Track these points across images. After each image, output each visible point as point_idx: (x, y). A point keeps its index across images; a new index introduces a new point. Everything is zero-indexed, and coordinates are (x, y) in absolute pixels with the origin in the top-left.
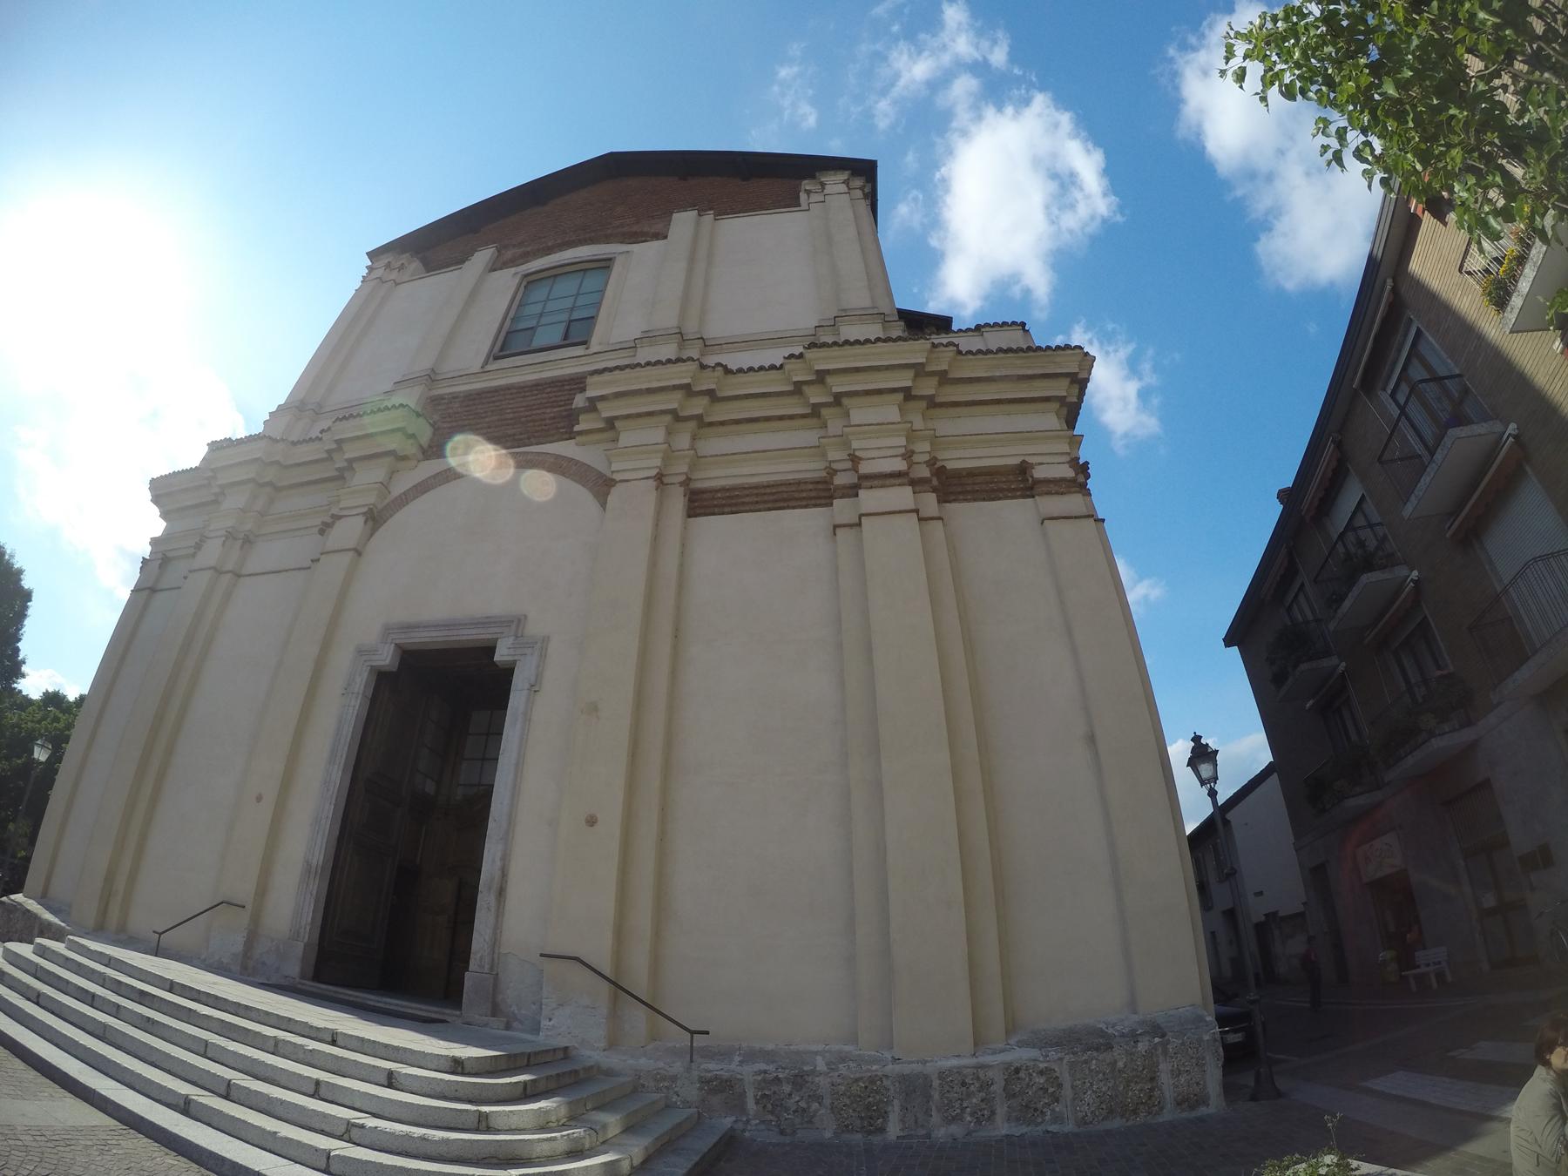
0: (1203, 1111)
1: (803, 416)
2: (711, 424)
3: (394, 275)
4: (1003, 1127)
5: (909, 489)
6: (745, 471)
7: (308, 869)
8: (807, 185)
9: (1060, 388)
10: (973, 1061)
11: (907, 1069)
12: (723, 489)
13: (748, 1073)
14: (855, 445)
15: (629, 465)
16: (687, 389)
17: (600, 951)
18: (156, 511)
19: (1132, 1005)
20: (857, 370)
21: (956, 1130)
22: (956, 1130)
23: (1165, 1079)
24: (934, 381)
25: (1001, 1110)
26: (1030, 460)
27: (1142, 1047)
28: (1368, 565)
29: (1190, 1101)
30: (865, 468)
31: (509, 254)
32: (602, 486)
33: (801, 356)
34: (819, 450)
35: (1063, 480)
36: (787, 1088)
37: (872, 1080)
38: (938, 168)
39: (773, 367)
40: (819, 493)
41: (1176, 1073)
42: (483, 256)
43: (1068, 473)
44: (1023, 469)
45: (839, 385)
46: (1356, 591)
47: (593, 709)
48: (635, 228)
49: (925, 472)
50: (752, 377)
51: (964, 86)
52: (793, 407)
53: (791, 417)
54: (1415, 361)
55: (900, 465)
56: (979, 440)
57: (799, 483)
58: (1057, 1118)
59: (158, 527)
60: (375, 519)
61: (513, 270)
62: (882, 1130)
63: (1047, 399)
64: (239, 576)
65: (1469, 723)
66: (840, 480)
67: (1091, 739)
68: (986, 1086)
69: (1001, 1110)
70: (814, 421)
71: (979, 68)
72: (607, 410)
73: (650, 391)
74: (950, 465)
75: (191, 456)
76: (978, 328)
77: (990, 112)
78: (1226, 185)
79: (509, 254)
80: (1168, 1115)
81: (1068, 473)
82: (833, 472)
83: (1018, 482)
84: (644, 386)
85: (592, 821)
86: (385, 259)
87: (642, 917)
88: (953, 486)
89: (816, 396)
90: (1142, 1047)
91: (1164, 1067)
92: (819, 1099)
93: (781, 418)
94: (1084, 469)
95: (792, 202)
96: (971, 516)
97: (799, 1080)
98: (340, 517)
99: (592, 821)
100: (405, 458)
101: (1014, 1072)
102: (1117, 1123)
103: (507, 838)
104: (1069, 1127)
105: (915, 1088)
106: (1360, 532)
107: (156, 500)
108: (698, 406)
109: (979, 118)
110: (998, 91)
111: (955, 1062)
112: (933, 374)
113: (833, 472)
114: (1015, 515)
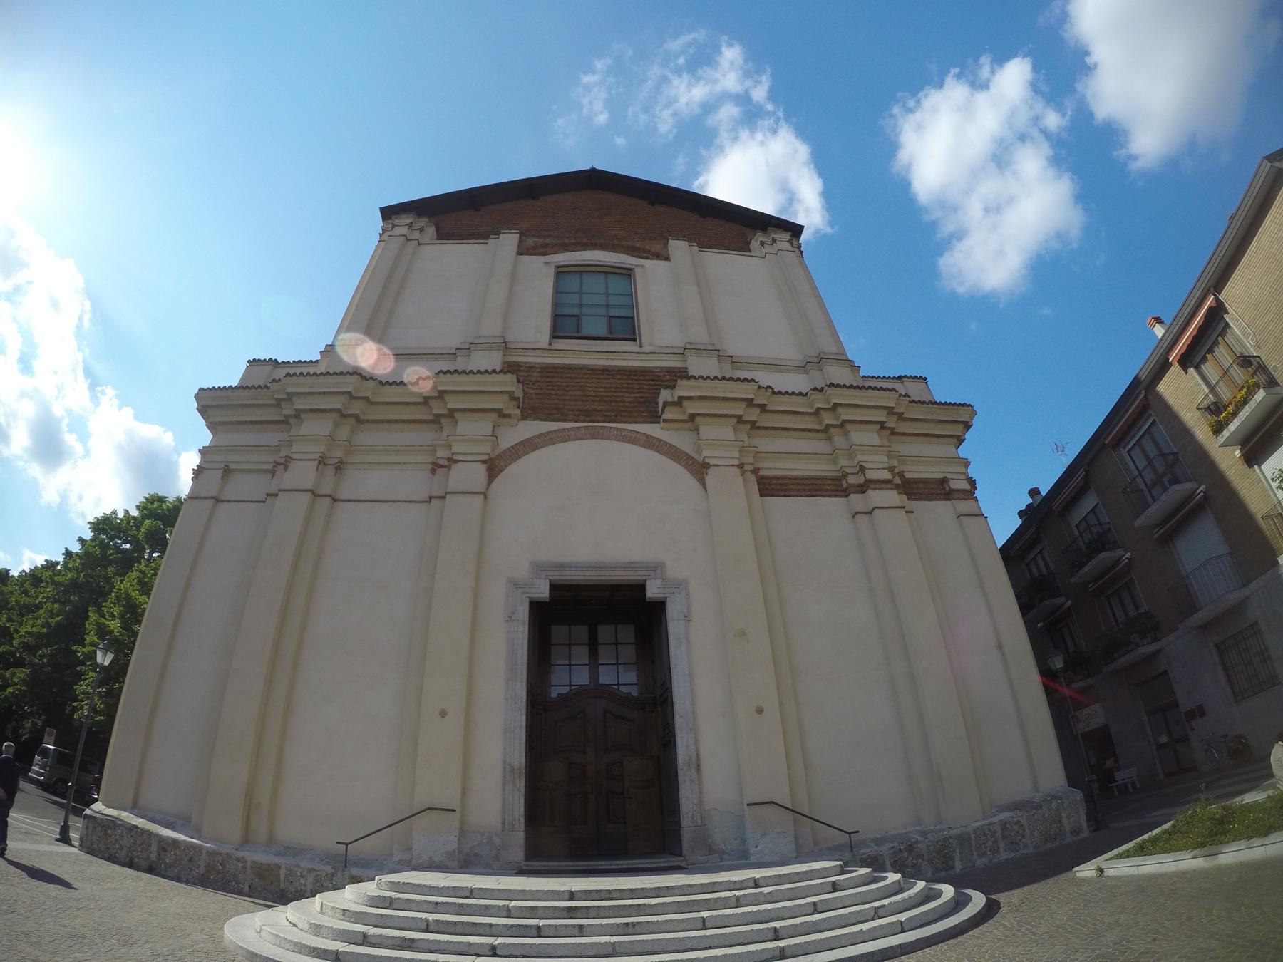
0: (1082, 836)
1: (817, 431)
2: (759, 428)
3: (416, 235)
4: (1004, 856)
5: (895, 492)
6: (788, 466)
7: (508, 769)
8: (760, 237)
9: (957, 430)
10: (986, 822)
11: (958, 831)
12: (776, 478)
13: (885, 849)
14: (860, 458)
15: (717, 454)
16: (750, 402)
18: (201, 422)
19: (1036, 788)
20: (857, 406)
21: (984, 860)
22: (984, 860)
23: (1065, 820)
24: (895, 418)
25: (1002, 846)
26: (949, 476)
27: (1054, 805)
28: (1103, 548)
29: (1076, 831)
31: (530, 242)
32: (699, 469)
33: (822, 390)
34: (832, 456)
35: (965, 490)
36: (905, 854)
37: (944, 840)
38: (825, 235)
39: (800, 394)
40: (835, 487)
41: (1069, 817)
42: (509, 240)
43: (968, 487)
44: (944, 481)
45: (845, 415)
46: (1094, 561)
47: (743, 634)
48: (638, 245)
49: (898, 481)
50: (786, 398)
51: (728, 112)
52: (809, 423)
53: (810, 430)
54: (1137, 448)
56: (923, 459)
57: (823, 478)
58: (1026, 846)
59: (206, 437)
60: (494, 467)
61: (542, 258)
62: (953, 867)
63: (951, 436)
64: (335, 500)
65: (1156, 640)
66: (852, 480)
67: (1000, 647)
68: (994, 833)
69: (1002, 846)
70: (823, 435)
71: (743, 99)
72: (691, 408)
73: (725, 399)
74: (908, 476)
75: (231, 376)
76: (900, 378)
77: (744, 134)
79: (530, 242)
80: (1068, 840)
81: (968, 487)
82: (845, 475)
83: (939, 490)
84: (721, 395)
86: (405, 220)
89: (828, 419)
90: (1054, 805)
91: (1064, 815)
92: (921, 856)
93: (803, 430)
94: (972, 482)
95: (744, 247)
96: (921, 506)
97: (911, 848)
98: (456, 461)
99: (760, 711)
100: (508, 416)
101: (1004, 825)
102: (1049, 845)
104: (1031, 850)
105: (964, 840)
107: (203, 410)
108: (753, 415)
109: (736, 139)
110: (751, 116)
111: (978, 824)
112: (896, 413)
113: (845, 475)
114: (941, 509)
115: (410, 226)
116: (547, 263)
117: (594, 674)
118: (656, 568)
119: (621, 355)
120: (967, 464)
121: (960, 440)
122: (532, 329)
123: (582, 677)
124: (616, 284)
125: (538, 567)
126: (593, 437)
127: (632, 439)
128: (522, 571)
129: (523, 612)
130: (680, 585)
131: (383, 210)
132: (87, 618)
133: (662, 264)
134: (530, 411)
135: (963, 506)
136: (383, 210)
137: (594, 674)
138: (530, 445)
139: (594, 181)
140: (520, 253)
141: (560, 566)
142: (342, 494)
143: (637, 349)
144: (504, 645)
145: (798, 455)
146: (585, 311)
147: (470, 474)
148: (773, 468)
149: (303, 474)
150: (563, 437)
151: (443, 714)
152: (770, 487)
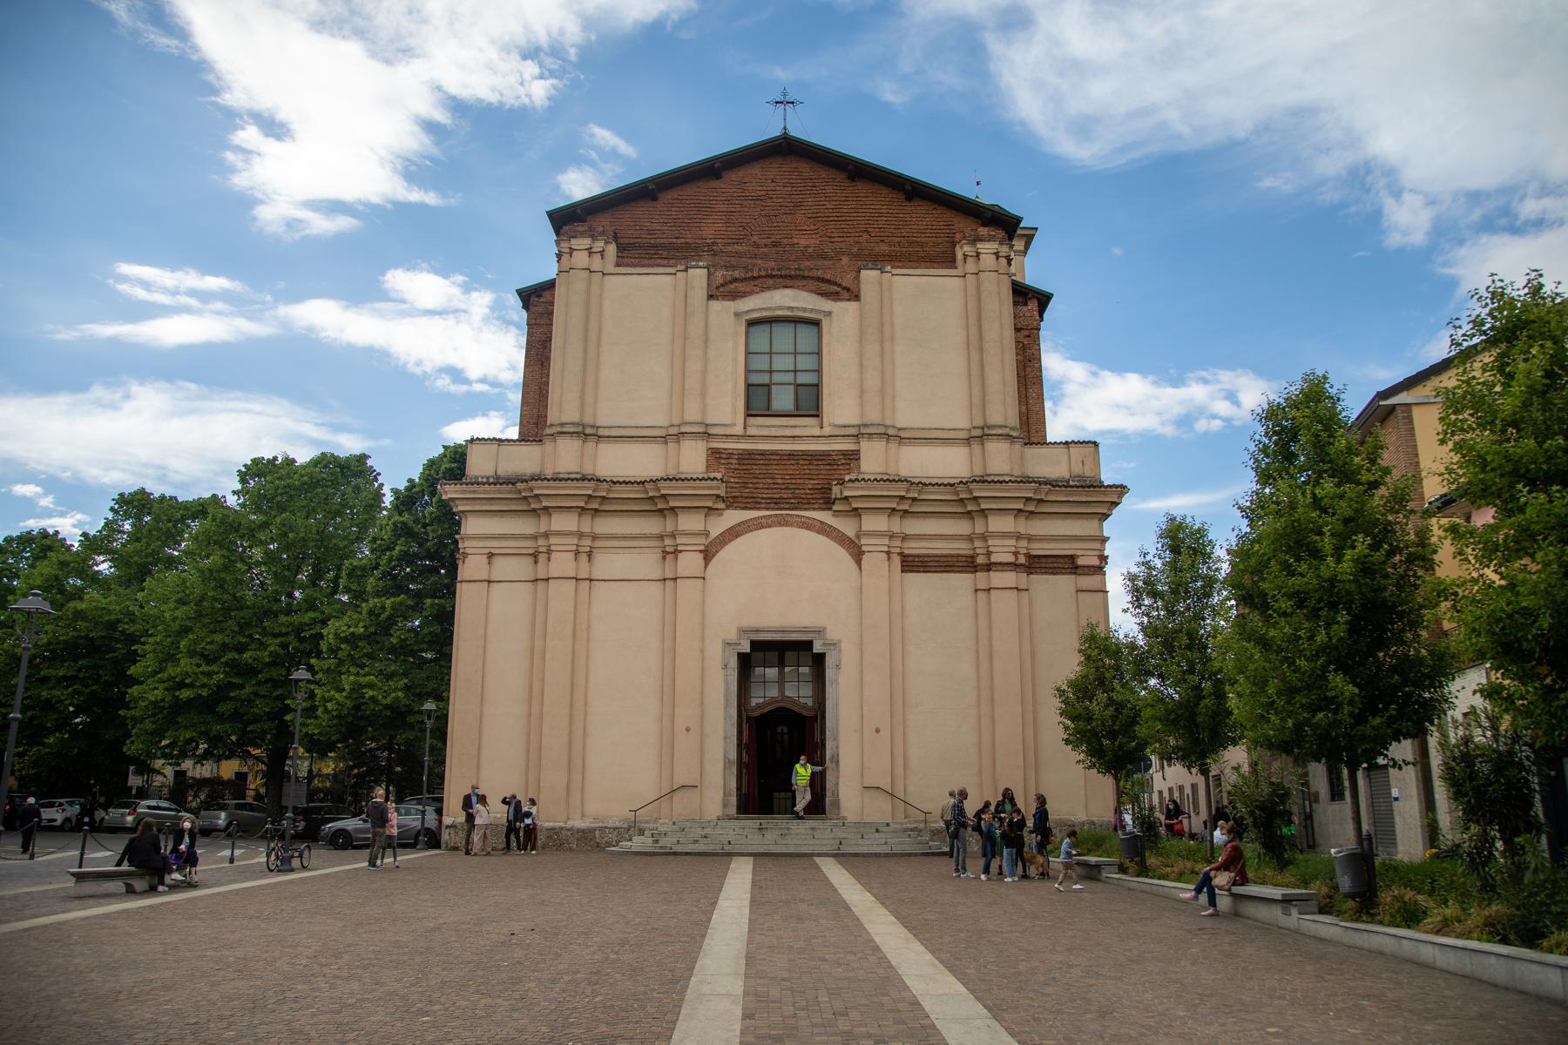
7: (727, 762)
17: (886, 785)
30: (994, 558)
32: (858, 554)
40: (969, 564)
44: (1072, 558)
49: (1022, 560)
55: (1011, 559)
56: (1054, 533)
60: (708, 555)
73: (586, 340)
78: (1104, 367)
81: (1096, 562)
83: (1069, 565)
85: (878, 731)
87: (899, 770)
88: (1035, 564)
94: (1104, 559)
99: (878, 731)
103: (836, 739)
106: (536, 71)
115: (590, 251)
116: (737, 315)
117: (782, 691)
118: (820, 632)
119: (803, 436)
120: (1104, 540)
121: (1106, 516)
122: (725, 407)
123: (773, 692)
124: (805, 335)
125: (743, 631)
126: (781, 525)
127: (808, 525)
128: (732, 636)
129: (734, 663)
130: (834, 645)
131: (552, 215)
132: (1206, 434)
133: (853, 305)
134: (732, 502)
135: (1087, 581)
136: (552, 215)
137: (782, 691)
138: (734, 533)
139: (785, 148)
140: (711, 297)
141: (758, 631)
142: (680, 573)
143: (817, 432)
144: (720, 684)
145: (941, 533)
146: (777, 378)
147: (690, 562)
148: (914, 548)
149: (562, 563)
150: (758, 525)
151: (688, 730)
152: (911, 564)
